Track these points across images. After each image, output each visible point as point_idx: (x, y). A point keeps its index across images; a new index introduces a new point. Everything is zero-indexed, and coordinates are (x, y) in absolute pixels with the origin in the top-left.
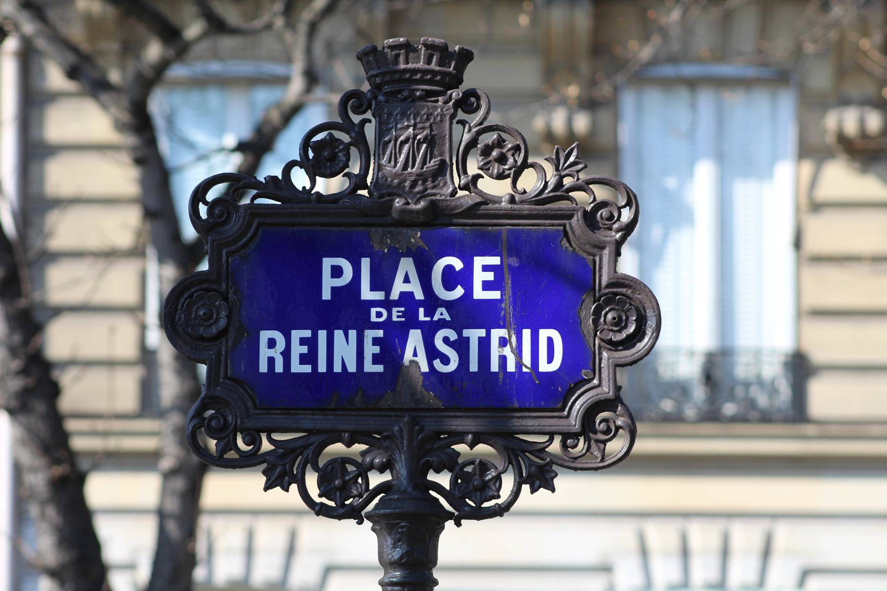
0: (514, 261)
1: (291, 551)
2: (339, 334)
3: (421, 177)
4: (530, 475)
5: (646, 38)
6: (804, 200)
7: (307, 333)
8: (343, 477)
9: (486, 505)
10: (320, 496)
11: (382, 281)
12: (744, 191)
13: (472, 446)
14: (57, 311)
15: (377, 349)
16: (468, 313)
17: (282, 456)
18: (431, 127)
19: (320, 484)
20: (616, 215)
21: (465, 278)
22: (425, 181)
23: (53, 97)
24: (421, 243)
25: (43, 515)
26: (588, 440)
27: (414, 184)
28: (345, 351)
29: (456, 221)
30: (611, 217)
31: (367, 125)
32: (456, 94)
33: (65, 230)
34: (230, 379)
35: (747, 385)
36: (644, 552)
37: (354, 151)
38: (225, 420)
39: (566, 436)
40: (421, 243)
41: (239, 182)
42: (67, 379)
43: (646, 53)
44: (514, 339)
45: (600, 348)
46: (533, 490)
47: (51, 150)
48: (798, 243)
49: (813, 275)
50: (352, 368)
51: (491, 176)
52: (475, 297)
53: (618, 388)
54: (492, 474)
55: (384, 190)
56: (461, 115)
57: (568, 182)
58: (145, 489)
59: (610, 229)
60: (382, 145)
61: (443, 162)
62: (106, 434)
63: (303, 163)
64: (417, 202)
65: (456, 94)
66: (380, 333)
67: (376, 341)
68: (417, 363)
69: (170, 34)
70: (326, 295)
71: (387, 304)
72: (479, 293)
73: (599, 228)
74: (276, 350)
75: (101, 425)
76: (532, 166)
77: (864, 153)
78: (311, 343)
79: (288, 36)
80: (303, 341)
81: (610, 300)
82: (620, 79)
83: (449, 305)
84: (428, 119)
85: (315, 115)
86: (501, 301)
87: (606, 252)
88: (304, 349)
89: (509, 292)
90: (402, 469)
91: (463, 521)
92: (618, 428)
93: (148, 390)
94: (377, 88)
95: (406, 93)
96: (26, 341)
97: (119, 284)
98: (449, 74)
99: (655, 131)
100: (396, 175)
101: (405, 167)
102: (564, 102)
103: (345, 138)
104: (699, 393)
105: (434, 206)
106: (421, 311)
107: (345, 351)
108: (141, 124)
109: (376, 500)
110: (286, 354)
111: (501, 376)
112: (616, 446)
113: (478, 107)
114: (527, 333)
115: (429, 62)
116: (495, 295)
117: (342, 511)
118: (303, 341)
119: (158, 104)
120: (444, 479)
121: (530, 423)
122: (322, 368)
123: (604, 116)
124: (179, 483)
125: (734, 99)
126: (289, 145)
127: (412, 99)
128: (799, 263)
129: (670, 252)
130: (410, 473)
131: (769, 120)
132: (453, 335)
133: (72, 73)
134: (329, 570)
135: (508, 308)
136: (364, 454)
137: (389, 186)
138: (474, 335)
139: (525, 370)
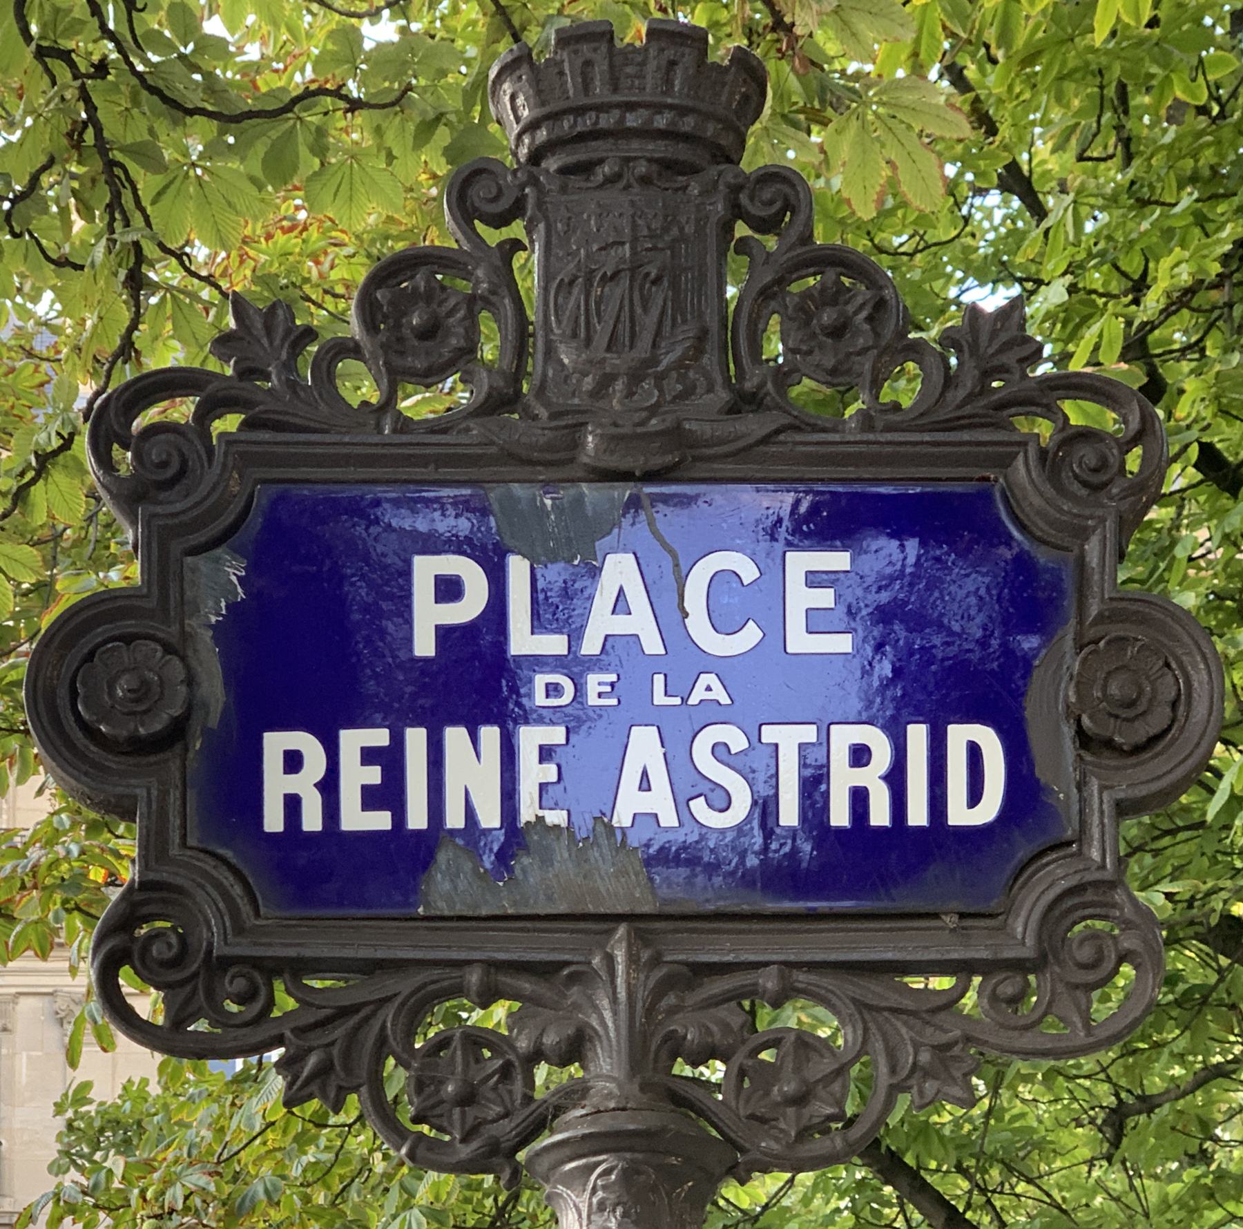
2: (455, 737)
7: (379, 737)
21: (767, 603)
31: (519, 259)
52: (266, 735)
78: (390, 759)
80: (369, 756)
83: (722, 667)
88: (373, 775)
110: (329, 786)
118: (369, 756)
122: (417, 818)
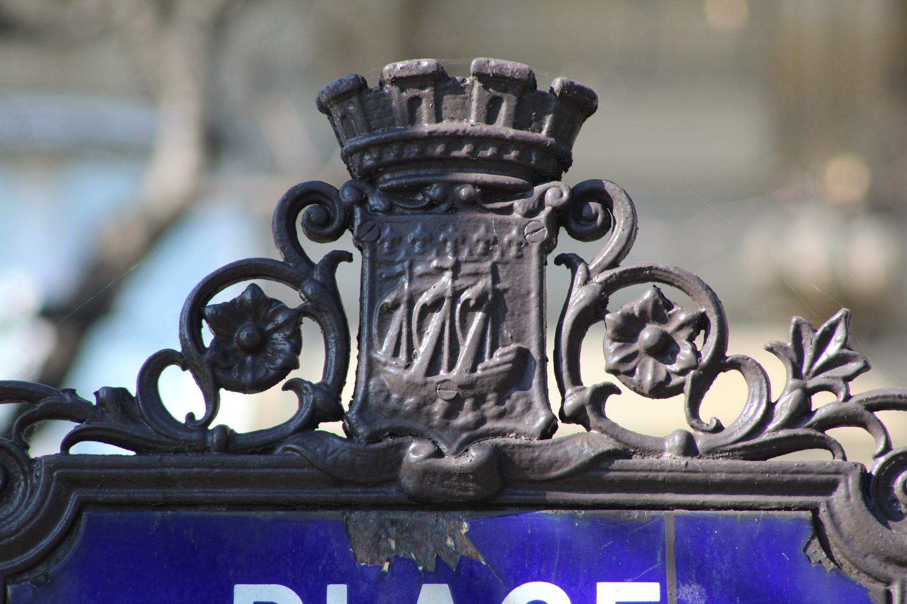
3: (472, 392)
22: (479, 401)
24: (470, 550)
27: (454, 408)
29: (553, 496)
32: (554, 193)
37: (310, 329)
40: (470, 550)
56: (566, 243)
60: (377, 313)
61: (523, 355)
63: (188, 357)
64: (462, 449)
65: (554, 193)
76: (736, 365)
84: (487, 253)
85: (228, 236)
94: (366, 178)
95: (435, 191)
98: (538, 145)
100: (412, 387)
101: (432, 367)
103: (290, 297)
105: (501, 462)
113: (607, 225)
115: (490, 118)
126: (153, 316)
127: (456, 206)
137: (395, 412)
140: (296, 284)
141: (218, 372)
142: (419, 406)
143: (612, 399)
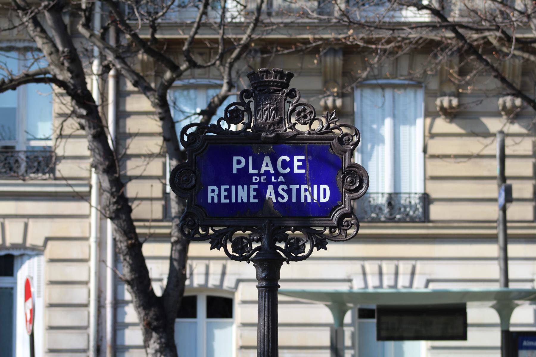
0: (310, 158)
1: (224, 274)
2: (240, 187)
3: (273, 124)
4: (316, 244)
5: (365, 69)
6: (427, 134)
7: (227, 187)
8: (242, 244)
9: (299, 255)
10: (233, 252)
11: (257, 165)
12: (404, 130)
13: (293, 232)
14: (131, 178)
15: (255, 193)
16: (292, 178)
17: (217, 236)
18: (276, 104)
19: (232, 247)
20: (351, 139)
21: (290, 164)
22: (274, 126)
23: (130, 93)
24: (273, 151)
25: (125, 259)
26: (340, 229)
27: (270, 127)
28: (242, 194)
29: (287, 141)
30: (349, 140)
32: (286, 91)
33: (134, 146)
34: (197, 205)
35: (405, 207)
36: (364, 274)
37: (245, 113)
38: (195, 222)
39: (331, 228)
40: (273, 151)
41: (202, 127)
42: (134, 205)
43: (364, 75)
44: (310, 189)
45: (345, 192)
46: (318, 250)
47: (129, 114)
48: (425, 151)
49: (431, 163)
50: (245, 201)
51: (301, 123)
53: (352, 208)
54: (302, 243)
55: (258, 129)
56: (289, 99)
57: (332, 125)
58: (165, 249)
59: (349, 144)
60: (257, 111)
61: (281, 118)
62: (150, 227)
63: (225, 118)
64: (271, 134)
65: (286, 91)
66: (256, 187)
67: (255, 190)
68: (271, 199)
69: (175, 68)
70: (235, 171)
71: (259, 175)
72: (296, 171)
73: (344, 144)
74: (215, 193)
75: (147, 224)
76: (317, 119)
77: (451, 114)
78: (229, 191)
79: (222, 68)
80: (225, 190)
81: (349, 173)
82: (354, 85)
83: (284, 175)
84: (275, 101)
85: (233, 99)
86: (305, 174)
87: (347, 154)
88: (226, 193)
89: (308, 170)
90: (265, 241)
91: (290, 262)
92: (352, 224)
93: (166, 209)
94: (255, 88)
95: (266, 90)
96: (118, 191)
97: (155, 167)
98: (284, 82)
99: (367, 104)
100: (263, 123)
101: (266, 120)
102: (332, 94)
103: (242, 109)
104: (386, 210)
105: (278, 135)
106: (273, 178)
107: (242, 194)
108: (163, 104)
109: (255, 254)
110: (219, 195)
111: (305, 204)
112: (351, 231)
113: (295, 96)
114: (315, 187)
115: (276, 78)
116: (303, 171)
117: (241, 258)
119: (170, 96)
120: (282, 246)
121: (317, 223)
122: (233, 201)
123: (348, 100)
124: (179, 247)
125: (400, 93)
126: (220, 112)
127: (270, 93)
128: (425, 158)
129: (375, 153)
130: (268, 242)
131: (414, 101)
132: (285, 187)
133: (135, 84)
134: (239, 281)
135: (308, 176)
136: (250, 235)
137: (260, 128)
138: (294, 187)
139: (314, 201)
140: (243, 106)
141: (230, 122)
142: (264, 127)
143: (196, 9)
